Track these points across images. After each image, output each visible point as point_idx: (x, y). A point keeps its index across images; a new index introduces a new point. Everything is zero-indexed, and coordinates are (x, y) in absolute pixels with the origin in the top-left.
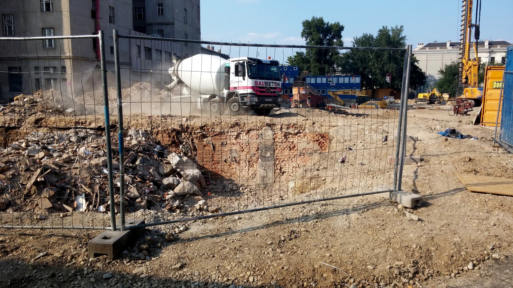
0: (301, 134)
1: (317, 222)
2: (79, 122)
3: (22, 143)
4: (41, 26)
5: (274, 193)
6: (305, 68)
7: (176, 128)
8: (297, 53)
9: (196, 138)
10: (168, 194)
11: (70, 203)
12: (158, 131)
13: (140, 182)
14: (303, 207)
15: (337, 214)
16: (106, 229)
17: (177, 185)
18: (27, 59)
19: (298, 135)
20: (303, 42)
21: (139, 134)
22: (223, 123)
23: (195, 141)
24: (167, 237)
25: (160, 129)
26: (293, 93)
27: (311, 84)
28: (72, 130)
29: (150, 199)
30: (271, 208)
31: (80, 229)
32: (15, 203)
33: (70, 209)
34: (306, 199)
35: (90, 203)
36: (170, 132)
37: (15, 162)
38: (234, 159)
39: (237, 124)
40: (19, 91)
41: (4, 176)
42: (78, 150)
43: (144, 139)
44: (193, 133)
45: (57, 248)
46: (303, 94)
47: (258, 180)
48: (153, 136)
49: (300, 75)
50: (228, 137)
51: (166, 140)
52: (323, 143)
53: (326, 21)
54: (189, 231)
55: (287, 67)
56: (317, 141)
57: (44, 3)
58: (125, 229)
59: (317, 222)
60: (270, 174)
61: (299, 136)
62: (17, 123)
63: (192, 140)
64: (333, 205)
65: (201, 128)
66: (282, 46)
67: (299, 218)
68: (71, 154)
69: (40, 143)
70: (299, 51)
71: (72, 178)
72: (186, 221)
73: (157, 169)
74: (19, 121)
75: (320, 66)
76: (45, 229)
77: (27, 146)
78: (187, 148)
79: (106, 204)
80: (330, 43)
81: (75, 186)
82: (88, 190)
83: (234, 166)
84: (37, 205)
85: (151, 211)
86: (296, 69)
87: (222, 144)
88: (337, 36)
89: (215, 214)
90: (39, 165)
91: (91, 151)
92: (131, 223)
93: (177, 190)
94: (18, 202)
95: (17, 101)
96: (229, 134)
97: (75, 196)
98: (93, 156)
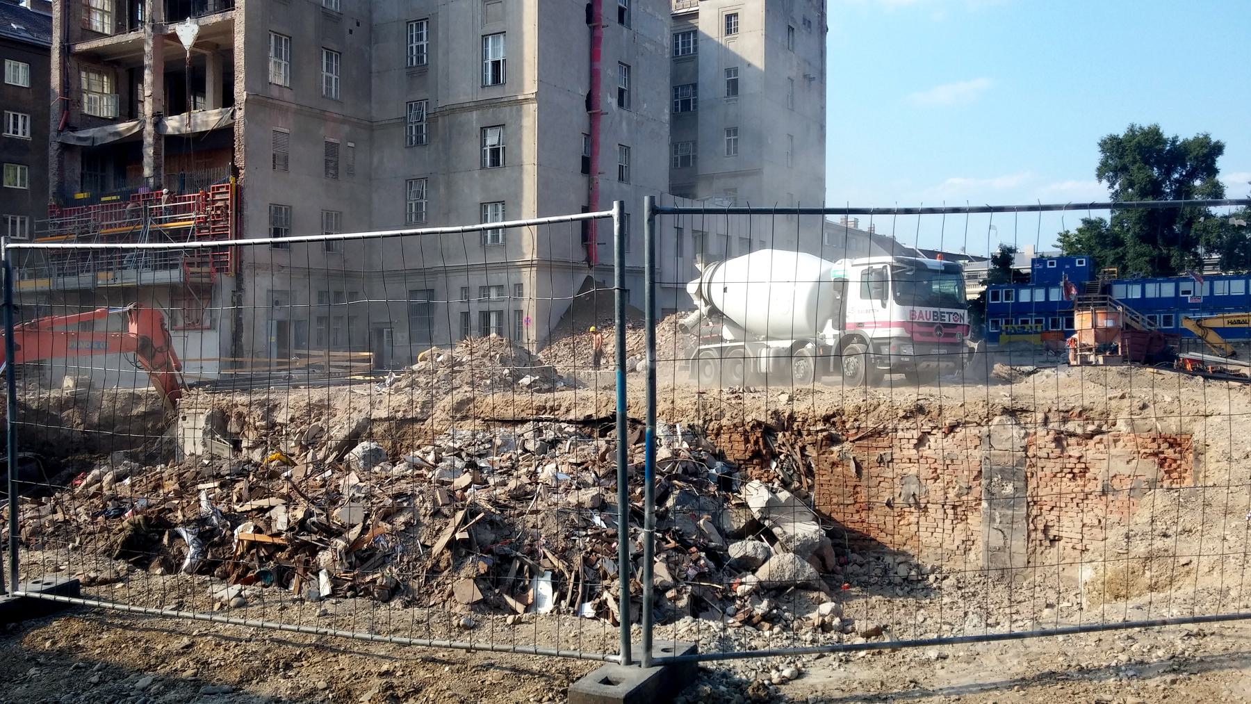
0: (1105, 437)
1: (1174, 682)
2: (545, 408)
3: (428, 453)
4: (479, 199)
5: (1028, 593)
6: (1111, 258)
7: (762, 419)
8: (1086, 221)
9: (814, 444)
10: (741, 584)
11: (519, 591)
12: (721, 428)
13: (675, 549)
14: (1129, 637)
15: (1236, 663)
16: (609, 661)
17: (764, 562)
18: (446, 271)
19: (1097, 438)
20: (1102, 192)
21: (675, 433)
22: (882, 407)
23: (812, 452)
24: (750, 691)
25: (724, 422)
26: (1077, 326)
27: (1126, 301)
28: (529, 426)
29: (698, 592)
30: (1032, 635)
31: (550, 655)
32: (407, 587)
33: (520, 608)
34: (1136, 617)
35: (562, 596)
36: (748, 428)
37: (413, 496)
38: (911, 500)
39: (920, 410)
40: (430, 341)
41: (389, 526)
42: (539, 470)
43: (686, 445)
44: (805, 433)
45: (499, 697)
46: (1107, 329)
47: (977, 557)
48: (708, 439)
49: (1093, 277)
50: (896, 442)
51: (736, 450)
52: (1175, 461)
53: (1168, 134)
54: (805, 680)
55: (1057, 259)
56: (1155, 454)
57: (488, 149)
58: (651, 663)
59: (1174, 682)
60: (1018, 544)
61: (1101, 441)
62: (422, 409)
63: (803, 449)
64: (1222, 636)
65: (827, 419)
66: (1058, 208)
67: (1117, 669)
68: (525, 480)
69: (464, 455)
70: (1093, 218)
71: (526, 534)
72: (797, 653)
73: (716, 520)
74: (424, 404)
75: (1155, 253)
76: (477, 649)
77: (438, 460)
78: (788, 469)
79: (597, 601)
80: (1183, 189)
81: (532, 553)
82: (560, 565)
83: (913, 519)
84: (451, 594)
85: (711, 623)
86: (1082, 263)
87: (881, 461)
88: (1204, 170)
89: (873, 640)
90: (459, 504)
91: (568, 474)
92: (664, 650)
93: (763, 573)
94: (414, 585)
95: (423, 363)
96: (900, 434)
97: (531, 577)
98: (571, 485)
